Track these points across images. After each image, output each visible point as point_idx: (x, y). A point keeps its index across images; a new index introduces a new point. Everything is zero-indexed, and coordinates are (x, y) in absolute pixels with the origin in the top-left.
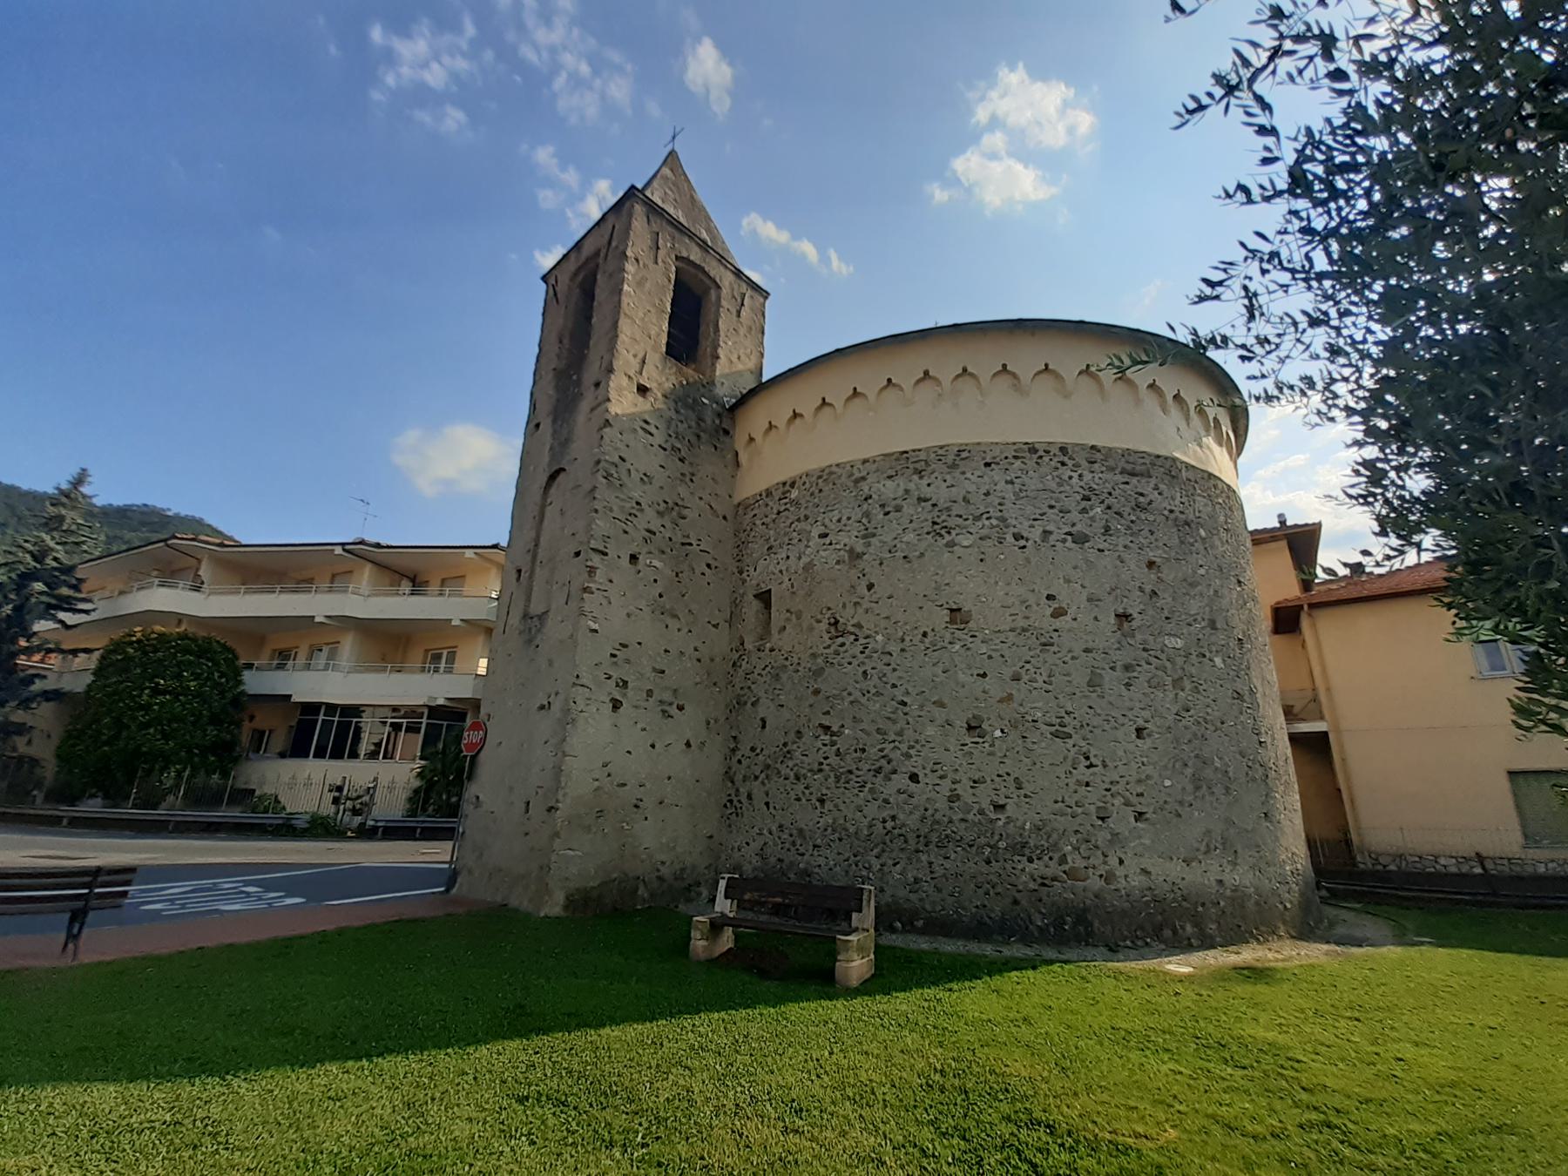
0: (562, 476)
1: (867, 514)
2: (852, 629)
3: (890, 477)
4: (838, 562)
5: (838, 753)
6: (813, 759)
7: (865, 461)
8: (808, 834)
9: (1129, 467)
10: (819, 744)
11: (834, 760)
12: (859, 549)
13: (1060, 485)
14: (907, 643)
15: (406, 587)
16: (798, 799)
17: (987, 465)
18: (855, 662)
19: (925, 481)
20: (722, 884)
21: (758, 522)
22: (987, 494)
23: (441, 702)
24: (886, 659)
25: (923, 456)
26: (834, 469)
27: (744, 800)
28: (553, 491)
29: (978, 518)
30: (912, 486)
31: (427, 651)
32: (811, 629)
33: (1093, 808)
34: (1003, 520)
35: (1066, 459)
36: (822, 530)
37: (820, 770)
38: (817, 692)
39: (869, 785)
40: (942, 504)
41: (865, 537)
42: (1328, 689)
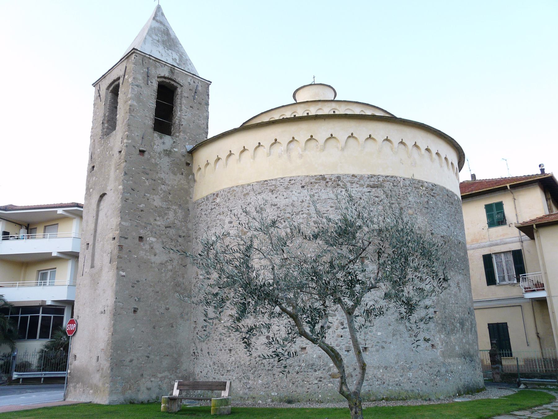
0: (105, 197)
7: (249, 185)
9: (371, 183)
15: (23, 232)
16: (221, 350)
17: (303, 187)
19: (274, 196)
20: (176, 385)
21: (203, 213)
23: (49, 303)
25: (274, 182)
26: (235, 188)
27: (199, 352)
28: (102, 203)
31: (39, 271)
33: (344, 347)
35: (340, 183)
40: (282, 208)
42: (546, 273)
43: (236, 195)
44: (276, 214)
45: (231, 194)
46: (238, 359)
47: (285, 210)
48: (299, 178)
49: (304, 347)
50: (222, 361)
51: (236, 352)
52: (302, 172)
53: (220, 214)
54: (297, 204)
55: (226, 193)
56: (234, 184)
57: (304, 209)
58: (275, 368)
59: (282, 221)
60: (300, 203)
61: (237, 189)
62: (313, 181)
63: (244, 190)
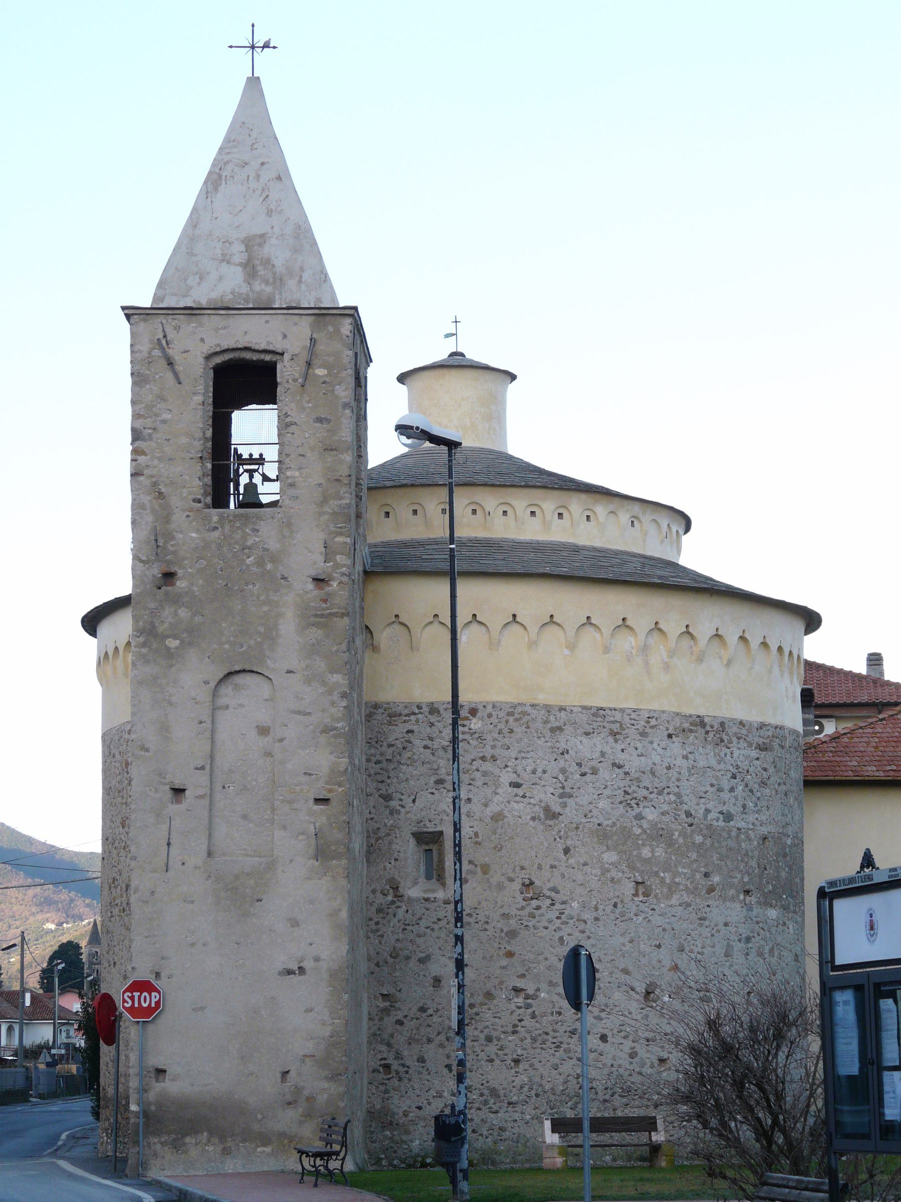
1: (563, 771)
2: (548, 893)
3: (587, 734)
4: (533, 819)
5: (533, 1016)
6: (507, 1020)
7: (562, 709)
8: (502, 1093)
10: (513, 1007)
11: (528, 1022)
12: (556, 808)
13: (719, 763)
14: (600, 912)
16: (491, 1061)
18: (551, 927)
19: (619, 746)
22: (669, 768)
24: (582, 926)
26: (528, 709)
29: (660, 793)
30: (607, 750)
32: (500, 887)
34: (678, 795)
36: (514, 778)
37: (514, 1032)
38: (510, 954)
39: (564, 1046)
40: (634, 775)
41: (561, 796)
43: (530, 724)
44: (622, 785)
45: (516, 720)
46: (537, 1079)
47: (638, 780)
48: (664, 717)
49: (665, 1057)
50: (494, 1084)
51: (532, 1065)
52: (667, 704)
53: (483, 758)
54: (661, 770)
55: (502, 714)
56: (523, 698)
57: (671, 785)
58: (616, 1096)
59: (633, 802)
60: (665, 771)
61: (534, 713)
62: (686, 725)
63: (552, 718)
